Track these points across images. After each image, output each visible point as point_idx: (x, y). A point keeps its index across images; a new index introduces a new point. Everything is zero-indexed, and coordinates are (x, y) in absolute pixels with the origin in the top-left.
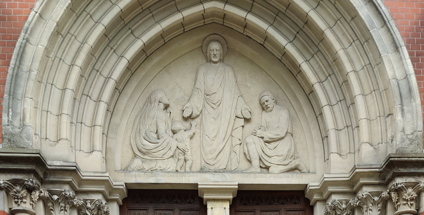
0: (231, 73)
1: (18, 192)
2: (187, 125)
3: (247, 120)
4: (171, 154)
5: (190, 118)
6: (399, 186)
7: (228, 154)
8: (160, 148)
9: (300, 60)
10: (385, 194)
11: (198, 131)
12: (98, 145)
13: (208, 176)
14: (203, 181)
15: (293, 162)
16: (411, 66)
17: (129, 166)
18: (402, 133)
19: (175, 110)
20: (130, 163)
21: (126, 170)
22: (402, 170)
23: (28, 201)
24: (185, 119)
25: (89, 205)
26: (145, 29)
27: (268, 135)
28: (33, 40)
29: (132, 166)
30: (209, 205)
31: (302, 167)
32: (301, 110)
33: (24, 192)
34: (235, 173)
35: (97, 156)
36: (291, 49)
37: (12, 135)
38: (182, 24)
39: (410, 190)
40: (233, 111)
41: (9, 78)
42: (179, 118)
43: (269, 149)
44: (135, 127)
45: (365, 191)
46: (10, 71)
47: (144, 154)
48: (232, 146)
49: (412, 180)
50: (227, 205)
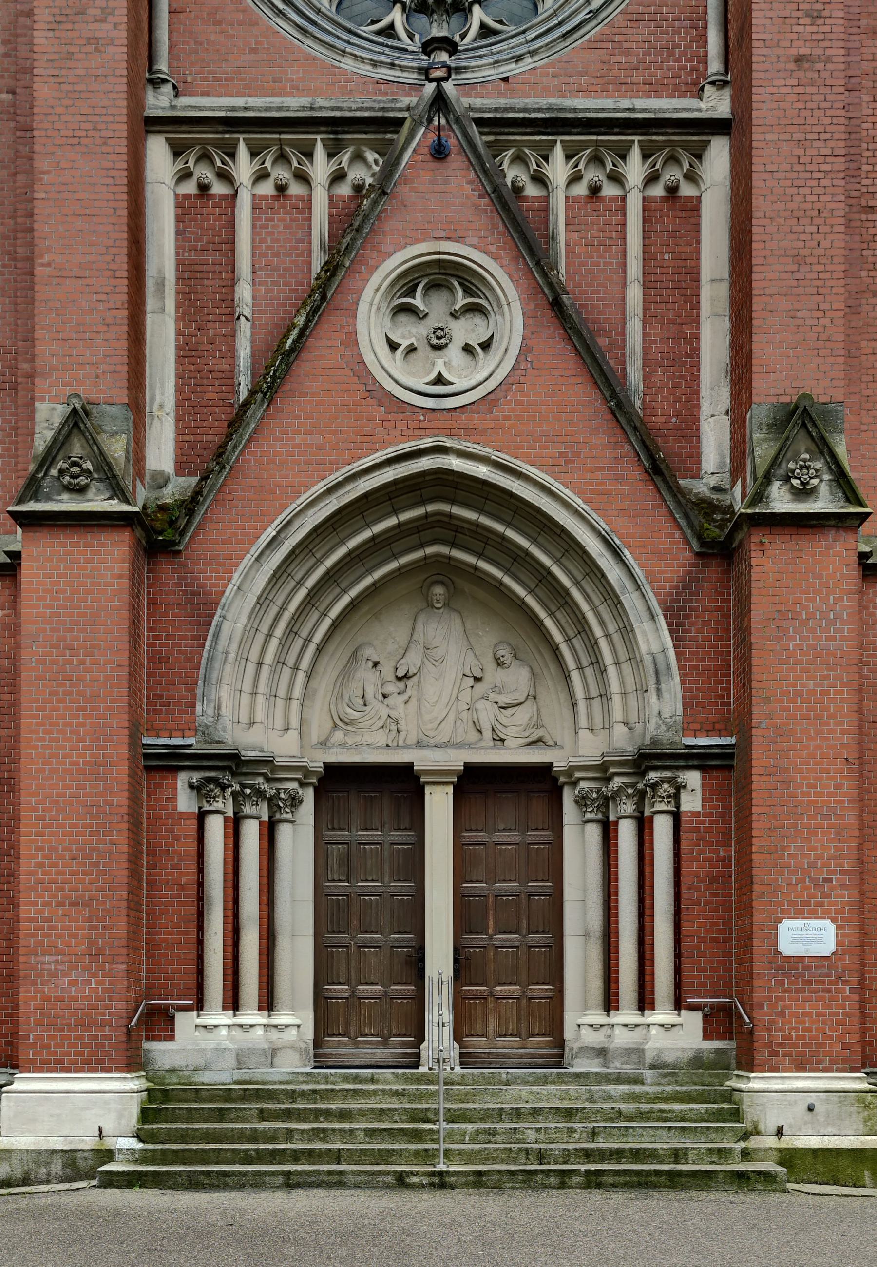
0: (458, 621)
1: (212, 791)
2: (401, 685)
3: (477, 680)
4: (381, 725)
5: (406, 676)
6: (652, 781)
7: (453, 722)
8: (367, 718)
9: (542, 614)
10: (640, 786)
11: (415, 693)
12: (295, 722)
15: (535, 733)
16: (670, 639)
17: (327, 739)
18: (658, 718)
19: (387, 670)
20: (329, 735)
21: (324, 744)
22: (656, 763)
23: (220, 799)
24: (399, 679)
25: (282, 795)
26: (352, 578)
27: (503, 699)
28: (229, 616)
29: (332, 740)
30: (427, 790)
31: (547, 739)
32: (547, 666)
33: (217, 791)
34: (460, 748)
36: (531, 601)
37: (207, 727)
38: (399, 569)
39: (666, 786)
40: (460, 668)
41: (203, 661)
42: (392, 677)
44: (337, 690)
45: (618, 781)
46: (205, 654)
47: (347, 724)
48: (458, 712)
49: (668, 774)
50: (450, 789)
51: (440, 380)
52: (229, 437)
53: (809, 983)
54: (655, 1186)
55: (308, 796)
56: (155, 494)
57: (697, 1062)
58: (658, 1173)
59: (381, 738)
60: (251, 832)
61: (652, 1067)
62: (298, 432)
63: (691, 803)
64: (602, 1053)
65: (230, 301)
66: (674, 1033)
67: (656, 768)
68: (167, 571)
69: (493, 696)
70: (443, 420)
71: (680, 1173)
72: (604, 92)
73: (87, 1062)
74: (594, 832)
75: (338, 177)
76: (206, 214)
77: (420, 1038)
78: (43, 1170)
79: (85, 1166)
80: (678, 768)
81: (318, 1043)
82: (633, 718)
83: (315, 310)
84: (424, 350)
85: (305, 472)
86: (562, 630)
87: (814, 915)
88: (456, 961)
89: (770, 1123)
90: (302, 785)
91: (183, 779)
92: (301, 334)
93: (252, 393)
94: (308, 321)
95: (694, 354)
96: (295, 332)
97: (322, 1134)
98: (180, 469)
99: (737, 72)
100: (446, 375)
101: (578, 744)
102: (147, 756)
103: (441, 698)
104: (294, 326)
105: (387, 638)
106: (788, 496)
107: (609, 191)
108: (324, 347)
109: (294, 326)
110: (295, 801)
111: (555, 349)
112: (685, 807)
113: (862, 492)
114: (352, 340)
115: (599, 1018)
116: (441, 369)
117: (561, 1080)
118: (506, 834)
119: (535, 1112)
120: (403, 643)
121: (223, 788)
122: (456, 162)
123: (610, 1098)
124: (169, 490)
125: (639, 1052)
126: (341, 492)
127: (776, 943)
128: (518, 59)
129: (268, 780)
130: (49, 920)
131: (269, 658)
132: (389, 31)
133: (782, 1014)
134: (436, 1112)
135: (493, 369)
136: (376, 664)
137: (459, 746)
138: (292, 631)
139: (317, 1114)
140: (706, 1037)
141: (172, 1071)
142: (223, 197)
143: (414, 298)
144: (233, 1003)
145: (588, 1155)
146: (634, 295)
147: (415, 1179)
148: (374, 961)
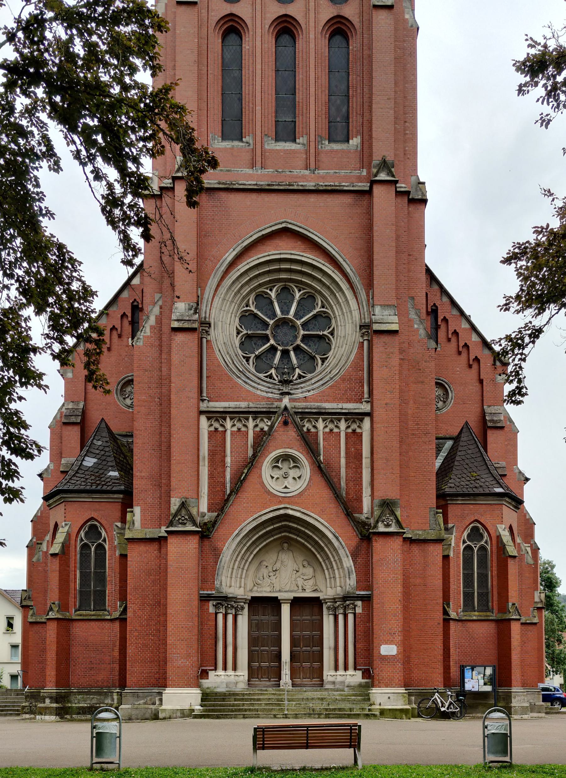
0: (291, 553)
2: (274, 573)
3: (297, 571)
5: (276, 570)
12: (243, 585)
13: (282, 594)
14: (280, 596)
21: (251, 591)
27: (305, 578)
30: (282, 605)
31: (318, 589)
35: (242, 589)
36: (313, 549)
43: (305, 583)
49: (352, 602)
50: (289, 605)
51: (286, 487)
52: (225, 505)
53: (389, 662)
54: (344, 718)
55: (246, 606)
56: (202, 519)
57: (360, 685)
58: (345, 714)
59: (268, 589)
60: (230, 618)
61: (347, 687)
62: (244, 503)
63: (359, 610)
64: (334, 683)
65: (223, 461)
66: (354, 677)
67: (348, 600)
68: (206, 542)
69: (302, 577)
70: (287, 500)
71: (351, 714)
72: (334, 401)
73: (186, 685)
74: (332, 618)
75: (256, 426)
76: (217, 437)
77: (280, 679)
78: (175, 715)
79: (189, 714)
80: (355, 600)
81: (249, 680)
82: (343, 585)
83: (249, 469)
84: (281, 478)
85: (247, 517)
86: (322, 558)
87: (390, 644)
88: (291, 656)
89: (377, 702)
90: (245, 603)
91: (211, 603)
92: (246, 475)
93: (231, 492)
94: (248, 471)
95: (361, 477)
96: (244, 475)
97: (253, 705)
98: (209, 510)
99: (371, 401)
100: (288, 486)
101: (328, 591)
102: (201, 597)
103: (286, 577)
104: (244, 473)
105: (270, 558)
106: (383, 526)
107: (336, 430)
108: (252, 478)
109: (244, 473)
110: (243, 608)
111: (319, 479)
112: (357, 612)
113: (404, 525)
114: (260, 476)
115: (333, 673)
116: (286, 484)
117: (320, 690)
118: (306, 617)
119: (313, 699)
120: (275, 560)
121: (223, 606)
122: (290, 426)
123: (334, 695)
124: (206, 517)
125: (344, 682)
126: (257, 520)
127: (380, 652)
128: (309, 391)
129: (235, 602)
130: (175, 645)
131: (236, 567)
132: (271, 377)
133: (382, 671)
134: (285, 699)
135: (301, 485)
136: (267, 567)
137: (291, 591)
138: (242, 558)
139: (251, 699)
140: (363, 678)
141: (208, 688)
142: (222, 431)
143: (271, 290)
144: (225, 668)
145: (326, 710)
146: (343, 461)
147: (278, 716)
148: (266, 656)
